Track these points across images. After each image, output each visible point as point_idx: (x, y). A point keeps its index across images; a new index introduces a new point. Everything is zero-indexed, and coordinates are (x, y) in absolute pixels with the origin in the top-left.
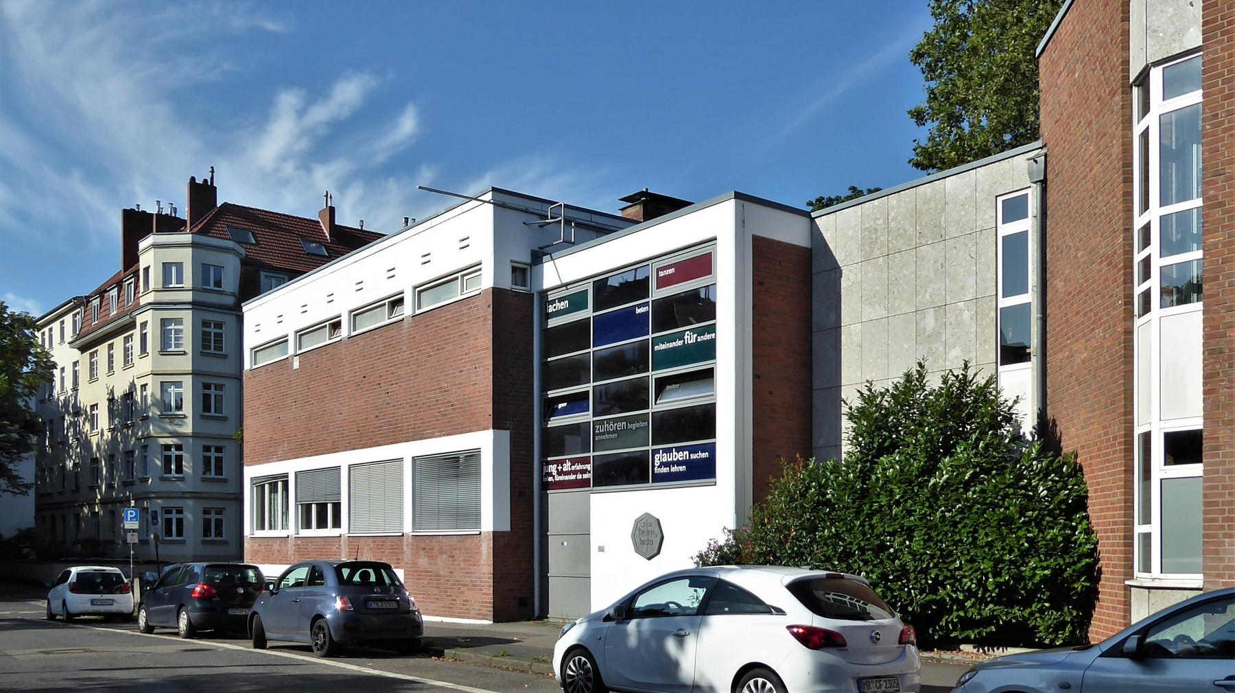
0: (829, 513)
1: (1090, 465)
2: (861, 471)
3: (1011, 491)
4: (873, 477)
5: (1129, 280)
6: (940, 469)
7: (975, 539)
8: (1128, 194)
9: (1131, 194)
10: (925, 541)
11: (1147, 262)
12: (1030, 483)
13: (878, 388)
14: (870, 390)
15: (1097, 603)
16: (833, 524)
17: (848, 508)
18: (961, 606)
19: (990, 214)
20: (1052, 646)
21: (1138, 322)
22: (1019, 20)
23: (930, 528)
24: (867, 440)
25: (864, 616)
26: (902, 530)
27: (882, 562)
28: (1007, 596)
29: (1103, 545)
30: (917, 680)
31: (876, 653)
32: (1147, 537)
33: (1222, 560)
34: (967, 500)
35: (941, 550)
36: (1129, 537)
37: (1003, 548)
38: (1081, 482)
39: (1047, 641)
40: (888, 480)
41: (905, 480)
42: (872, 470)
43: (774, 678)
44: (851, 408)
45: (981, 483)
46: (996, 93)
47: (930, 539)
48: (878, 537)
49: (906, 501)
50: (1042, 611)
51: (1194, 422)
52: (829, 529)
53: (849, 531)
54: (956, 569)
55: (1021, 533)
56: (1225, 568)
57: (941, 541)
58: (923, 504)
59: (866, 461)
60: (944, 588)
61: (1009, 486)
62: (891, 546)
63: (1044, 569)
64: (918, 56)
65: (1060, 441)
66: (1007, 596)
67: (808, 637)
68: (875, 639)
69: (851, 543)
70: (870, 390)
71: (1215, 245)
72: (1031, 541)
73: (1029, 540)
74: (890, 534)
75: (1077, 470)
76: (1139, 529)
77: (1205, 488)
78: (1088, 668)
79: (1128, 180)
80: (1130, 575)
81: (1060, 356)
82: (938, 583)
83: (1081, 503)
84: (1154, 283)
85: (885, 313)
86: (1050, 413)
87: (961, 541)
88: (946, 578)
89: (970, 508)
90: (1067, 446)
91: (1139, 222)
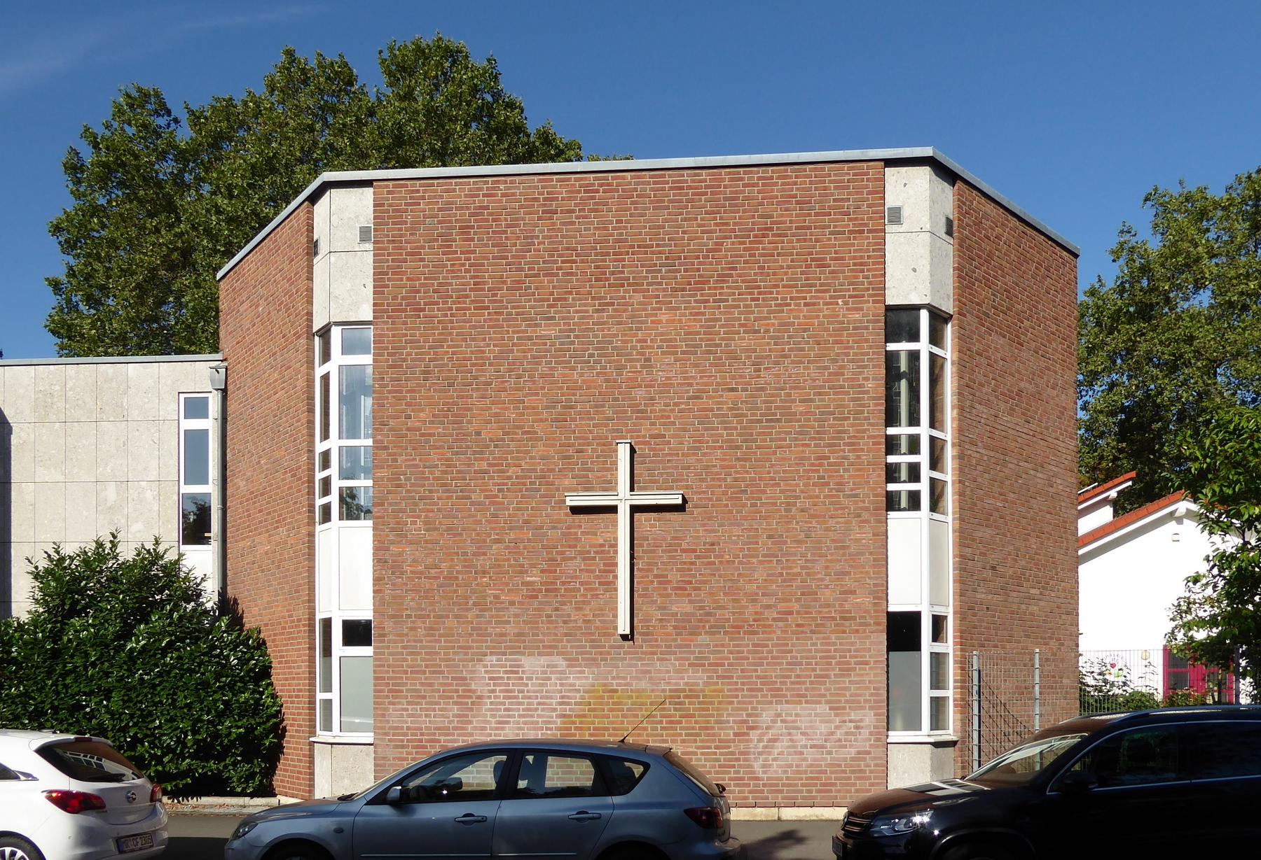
0: (16, 672)
1: (274, 641)
2: (51, 631)
3: (206, 659)
4: (65, 639)
5: (311, 492)
6: (135, 635)
7: (174, 701)
8: (311, 423)
9: (313, 423)
10: (125, 702)
11: (326, 482)
12: (222, 653)
13: (69, 549)
14: (58, 553)
15: (282, 757)
16: (20, 683)
17: (38, 668)
18: (159, 760)
19: (172, 408)
20: (243, 794)
21: (319, 528)
22: (157, 230)
23: (130, 690)
24: (57, 601)
25: (117, 778)
26: (100, 690)
27: (78, 721)
28: (204, 752)
29: (288, 708)
30: (166, 835)
31: (129, 813)
32: (328, 704)
33: (388, 722)
34: (165, 665)
35: (140, 709)
36: (312, 702)
37: (201, 710)
38: (264, 654)
39: (239, 790)
40: (81, 642)
41: (99, 641)
42: (62, 630)
43: (26, 845)
44: (36, 568)
45: (178, 650)
46: (135, 289)
47: (130, 700)
48: (73, 696)
49: (102, 663)
50: (235, 764)
51: (364, 612)
52: (17, 687)
53: (40, 690)
54: (156, 728)
55: (217, 696)
56: (390, 728)
57: (141, 702)
58: (121, 667)
59: (56, 622)
60: (143, 745)
61: (204, 654)
62: (87, 706)
63: (239, 727)
64: (57, 229)
65: (242, 617)
66: (204, 752)
67: (64, 801)
68: (131, 800)
69: (43, 702)
70: (58, 553)
71: (382, 478)
72: (226, 703)
73: (224, 703)
74: (85, 694)
75: (261, 644)
76: (320, 696)
77: (375, 666)
78: (357, 814)
79: (311, 411)
80: (313, 733)
81: (241, 544)
82: (136, 741)
83: (265, 672)
84: (334, 499)
85: (62, 478)
86: (230, 592)
87: (160, 702)
88: (146, 736)
89: (169, 672)
90: (250, 622)
91: (320, 447)
